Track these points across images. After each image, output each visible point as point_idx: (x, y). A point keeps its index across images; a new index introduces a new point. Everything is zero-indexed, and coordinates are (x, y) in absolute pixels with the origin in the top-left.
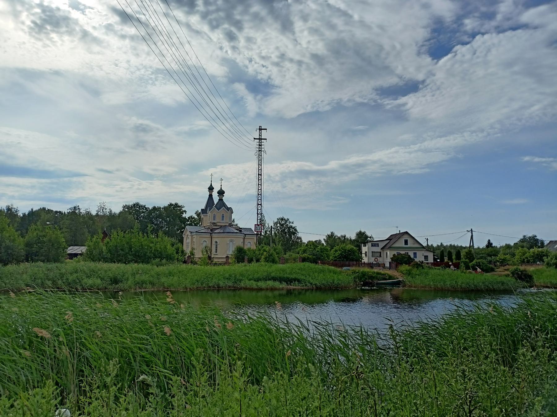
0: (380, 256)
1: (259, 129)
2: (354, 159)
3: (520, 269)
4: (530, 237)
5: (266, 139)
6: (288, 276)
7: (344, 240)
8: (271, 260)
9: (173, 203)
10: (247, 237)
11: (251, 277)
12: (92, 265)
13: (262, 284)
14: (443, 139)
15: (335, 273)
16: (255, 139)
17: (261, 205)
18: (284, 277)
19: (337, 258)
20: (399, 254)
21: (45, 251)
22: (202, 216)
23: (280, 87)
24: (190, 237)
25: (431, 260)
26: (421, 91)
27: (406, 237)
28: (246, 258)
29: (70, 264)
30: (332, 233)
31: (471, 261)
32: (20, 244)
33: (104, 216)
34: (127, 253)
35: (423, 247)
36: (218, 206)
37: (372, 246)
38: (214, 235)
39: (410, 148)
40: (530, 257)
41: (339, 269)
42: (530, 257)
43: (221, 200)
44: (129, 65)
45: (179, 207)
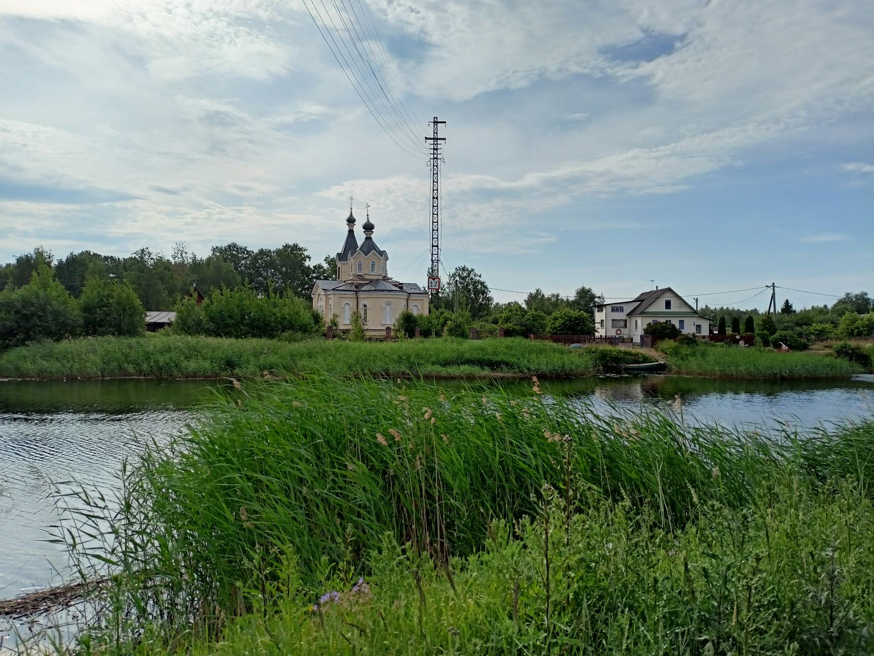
0: (626, 326)
1: (434, 122)
2: (565, 170)
3: (849, 346)
4: (857, 296)
5: (445, 139)
6: (490, 357)
7: (556, 302)
8: (459, 332)
9: (291, 243)
10: (412, 297)
11: (433, 359)
12: (192, 340)
13: (452, 370)
14: (712, 135)
15: (562, 352)
16: (426, 138)
17: (437, 246)
18: (485, 360)
19: (558, 330)
20: (656, 323)
21: (114, 318)
22: (339, 264)
23: (439, 47)
24: (324, 298)
25: (705, 332)
26: (678, 53)
27: (668, 297)
28: (417, 330)
29: (155, 341)
30: (537, 291)
31: (773, 333)
32: (73, 308)
33: (182, 265)
34: (238, 322)
35: (695, 312)
36: (365, 249)
37: (613, 310)
38: (361, 295)
39: (658, 151)
40: (863, 327)
41: (566, 347)
42: (863, 327)
43: (368, 239)
44: (191, 12)
45: (300, 249)
